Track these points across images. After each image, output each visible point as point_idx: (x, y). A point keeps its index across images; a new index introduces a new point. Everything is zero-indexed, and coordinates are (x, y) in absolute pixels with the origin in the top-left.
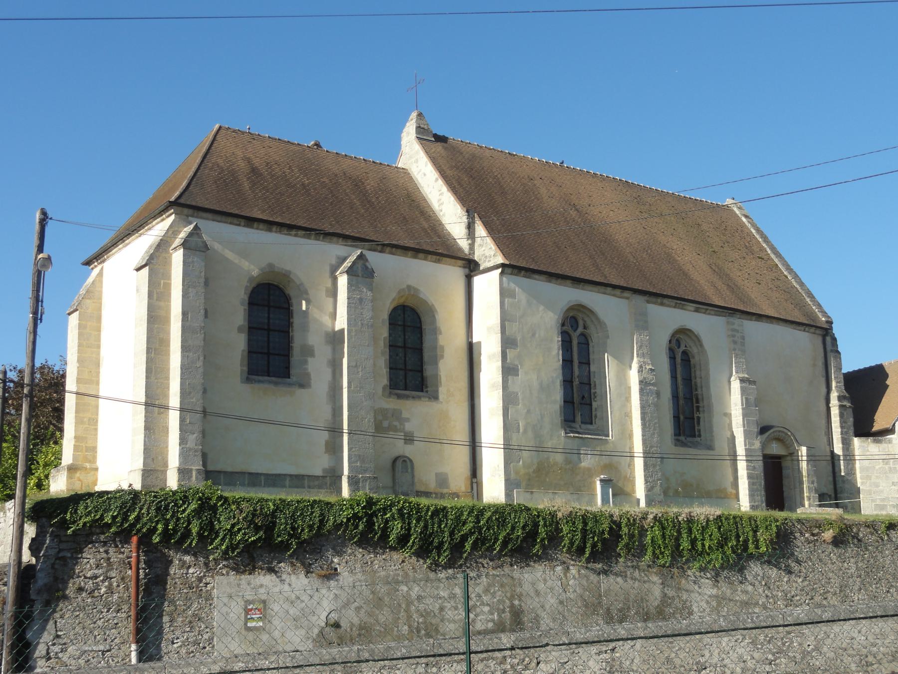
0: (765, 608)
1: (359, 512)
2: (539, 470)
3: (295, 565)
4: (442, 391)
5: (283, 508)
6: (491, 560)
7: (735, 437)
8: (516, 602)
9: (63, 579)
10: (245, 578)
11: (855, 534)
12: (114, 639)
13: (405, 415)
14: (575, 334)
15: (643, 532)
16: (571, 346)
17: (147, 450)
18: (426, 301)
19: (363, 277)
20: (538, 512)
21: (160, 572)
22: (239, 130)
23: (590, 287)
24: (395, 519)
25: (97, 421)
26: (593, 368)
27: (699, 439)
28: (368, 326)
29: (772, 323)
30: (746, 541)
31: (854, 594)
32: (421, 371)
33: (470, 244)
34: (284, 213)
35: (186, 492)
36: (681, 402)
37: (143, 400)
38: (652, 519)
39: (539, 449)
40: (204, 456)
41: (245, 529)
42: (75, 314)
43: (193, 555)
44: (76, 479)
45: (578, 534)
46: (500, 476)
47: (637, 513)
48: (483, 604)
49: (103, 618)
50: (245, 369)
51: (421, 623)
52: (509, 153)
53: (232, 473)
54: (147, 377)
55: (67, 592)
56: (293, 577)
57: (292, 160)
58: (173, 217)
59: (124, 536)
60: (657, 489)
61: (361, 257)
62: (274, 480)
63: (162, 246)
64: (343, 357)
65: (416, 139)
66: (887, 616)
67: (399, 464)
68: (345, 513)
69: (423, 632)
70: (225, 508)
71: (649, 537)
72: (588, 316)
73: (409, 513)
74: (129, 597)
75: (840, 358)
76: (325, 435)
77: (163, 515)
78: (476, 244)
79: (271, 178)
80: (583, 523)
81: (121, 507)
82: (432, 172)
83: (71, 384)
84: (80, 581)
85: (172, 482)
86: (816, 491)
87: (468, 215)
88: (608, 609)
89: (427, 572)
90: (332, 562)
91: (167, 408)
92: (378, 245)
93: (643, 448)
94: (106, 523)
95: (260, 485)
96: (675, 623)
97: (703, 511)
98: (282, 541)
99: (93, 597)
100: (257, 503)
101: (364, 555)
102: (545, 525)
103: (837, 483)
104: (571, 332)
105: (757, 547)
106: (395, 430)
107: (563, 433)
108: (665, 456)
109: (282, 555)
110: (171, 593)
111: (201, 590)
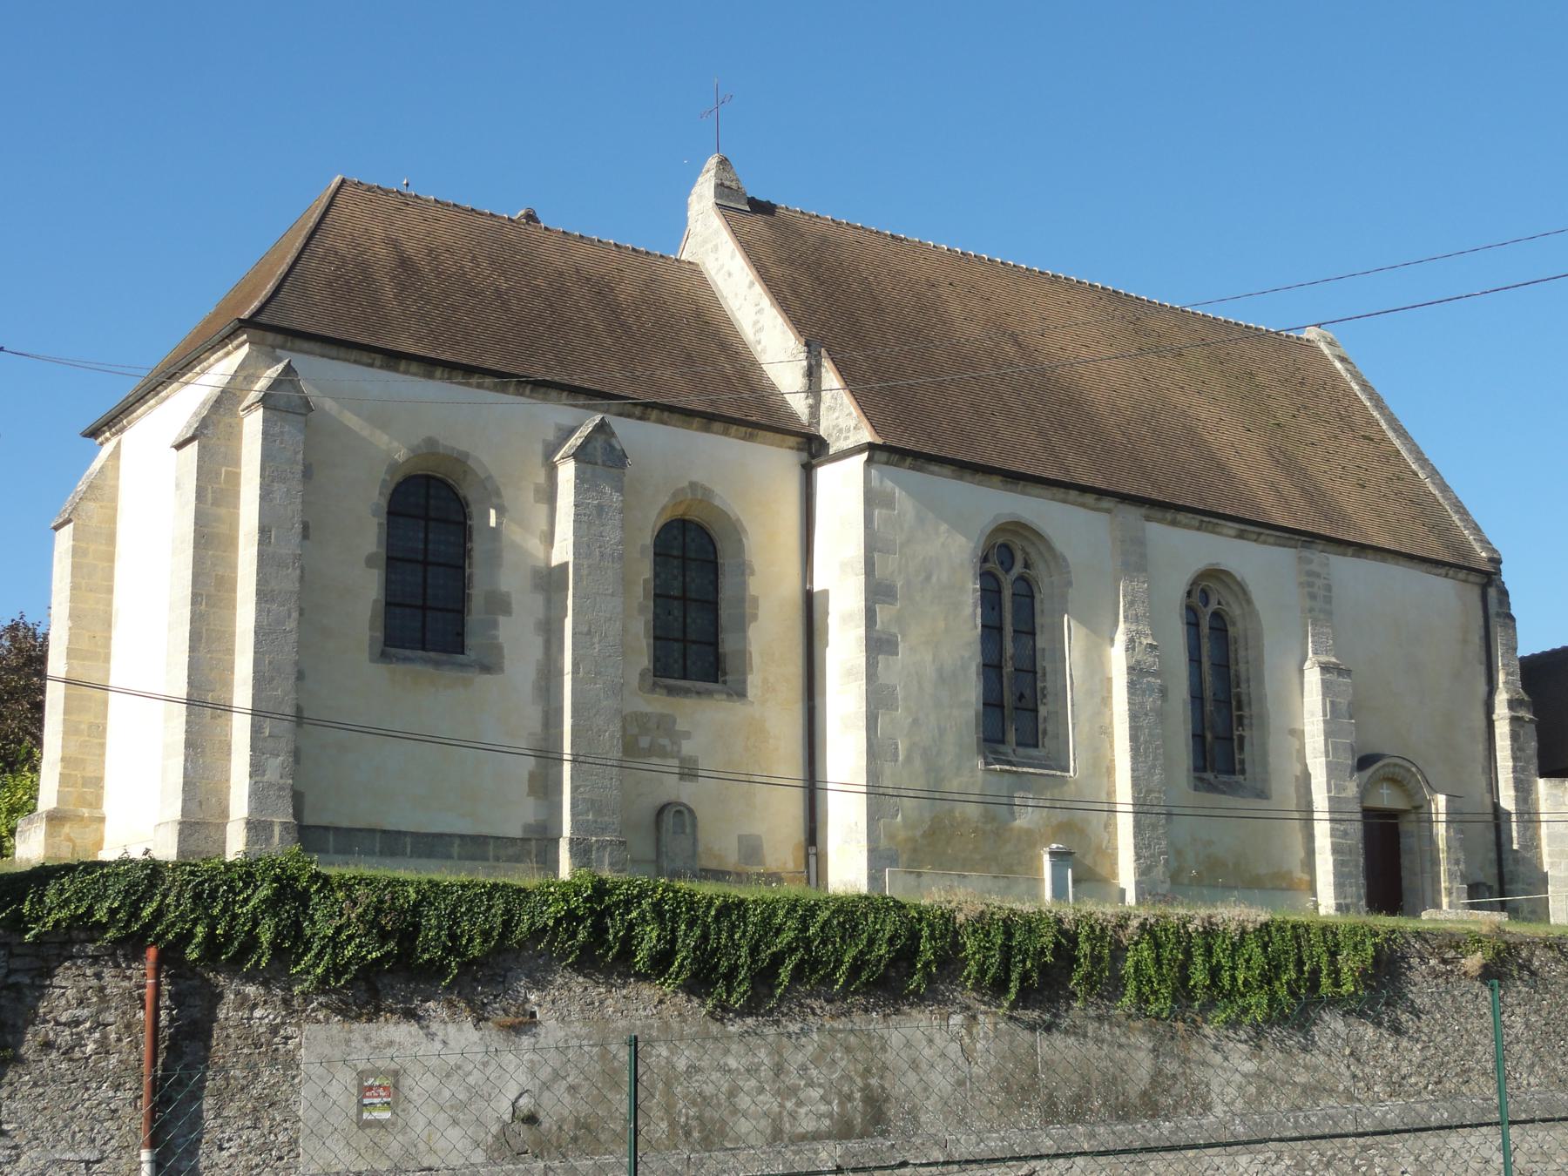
0: (1351, 1098)
1: (578, 907)
2: (934, 833)
3: (456, 1007)
4: (754, 682)
5: (435, 898)
6: (829, 1001)
7: (1310, 775)
8: (874, 1082)
9: (14, 1026)
10: (360, 1028)
11: (1524, 960)
12: (110, 1139)
13: (682, 725)
14: (1008, 577)
15: (1119, 953)
16: (1000, 599)
17: (189, 786)
18: (726, 513)
19: (604, 465)
20: (920, 913)
21: (199, 1015)
22: (378, 187)
23: (1038, 490)
24: (647, 921)
25: (105, 729)
26: (1041, 642)
27: (1242, 777)
28: (613, 558)
29: (1384, 560)
30: (1316, 972)
31: (1521, 1074)
32: (714, 643)
33: (811, 406)
34: (458, 343)
35: (251, 865)
36: (1209, 707)
37: (182, 690)
38: (1137, 928)
39: (934, 794)
40: (298, 799)
41: (360, 936)
42: (66, 527)
43: (262, 984)
44: (62, 838)
45: (994, 955)
46: (859, 842)
47: (1109, 917)
48: (810, 1084)
49: (89, 1100)
50: (380, 635)
51: (693, 1117)
52: (892, 236)
53: (350, 831)
54: (192, 649)
55: (23, 1050)
56: (451, 1028)
57: (479, 244)
58: (246, 349)
59: (132, 946)
60: (1159, 872)
61: (602, 427)
62: (430, 845)
63: (225, 402)
64: (566, 615)
65: (716, 208)
66: (1553, 1120)
67: (669, 819)
68: (552, 909)
69: (696, 1134)
70: (325, 897)
71: (1130, 963)
72: (1033, 544)
73: (673, 911)
74: (139, 1060)
75: (1514, 628)
76: (530, 763)
77: (206, 908)
78: (822, 405)
79: (437, 277)
80: (1005, 933)
81: (127, 892)
82: (743, 269)
83: (56, 664)
84: (47, 1030)
85: (235, 845)
86: (1464, 878)
87: (809, 352)
88: (1050, 1096)
89: (705, 1022)
90: (527, 1000)
91: (229, 709)
92: (635, 405)
93: (1133, 793)
94: (98, 922)
95: (404, 854)
96: (1148, 1126)
97: (1235, 914)
98: (431, 960)
99: (71, 1060)
100: (386, 887)
101: (586, 989)
102: (932, 937)
103: (1504, 863)
104: (1000, 574)
105: (1337, 983)
106: (663, 753)
107: (980, 764)
108: (1176, 811)
109: (432, 986)
110: (220, 1054)
111: (277, 1049)
